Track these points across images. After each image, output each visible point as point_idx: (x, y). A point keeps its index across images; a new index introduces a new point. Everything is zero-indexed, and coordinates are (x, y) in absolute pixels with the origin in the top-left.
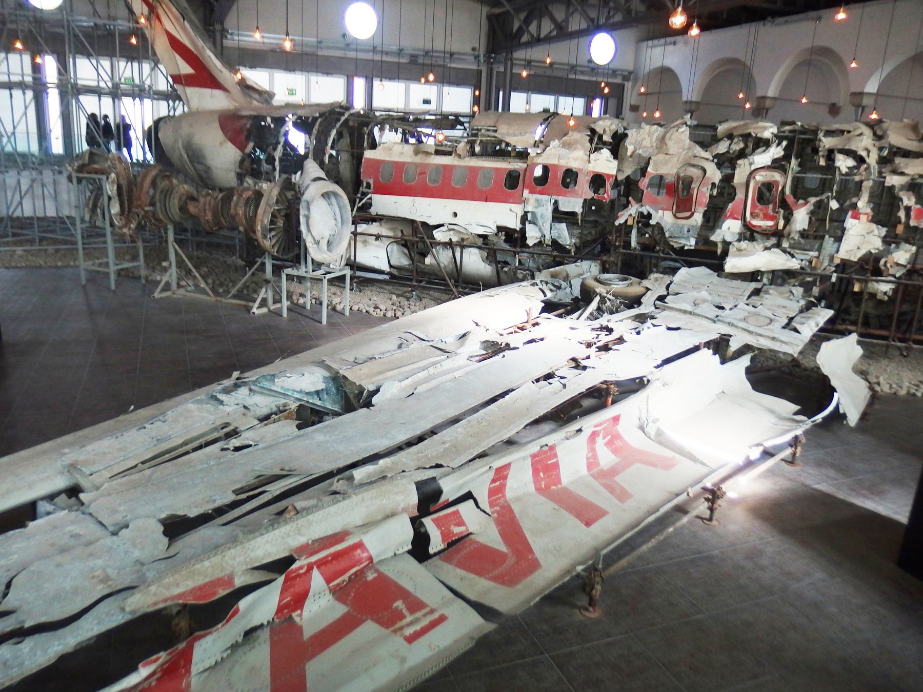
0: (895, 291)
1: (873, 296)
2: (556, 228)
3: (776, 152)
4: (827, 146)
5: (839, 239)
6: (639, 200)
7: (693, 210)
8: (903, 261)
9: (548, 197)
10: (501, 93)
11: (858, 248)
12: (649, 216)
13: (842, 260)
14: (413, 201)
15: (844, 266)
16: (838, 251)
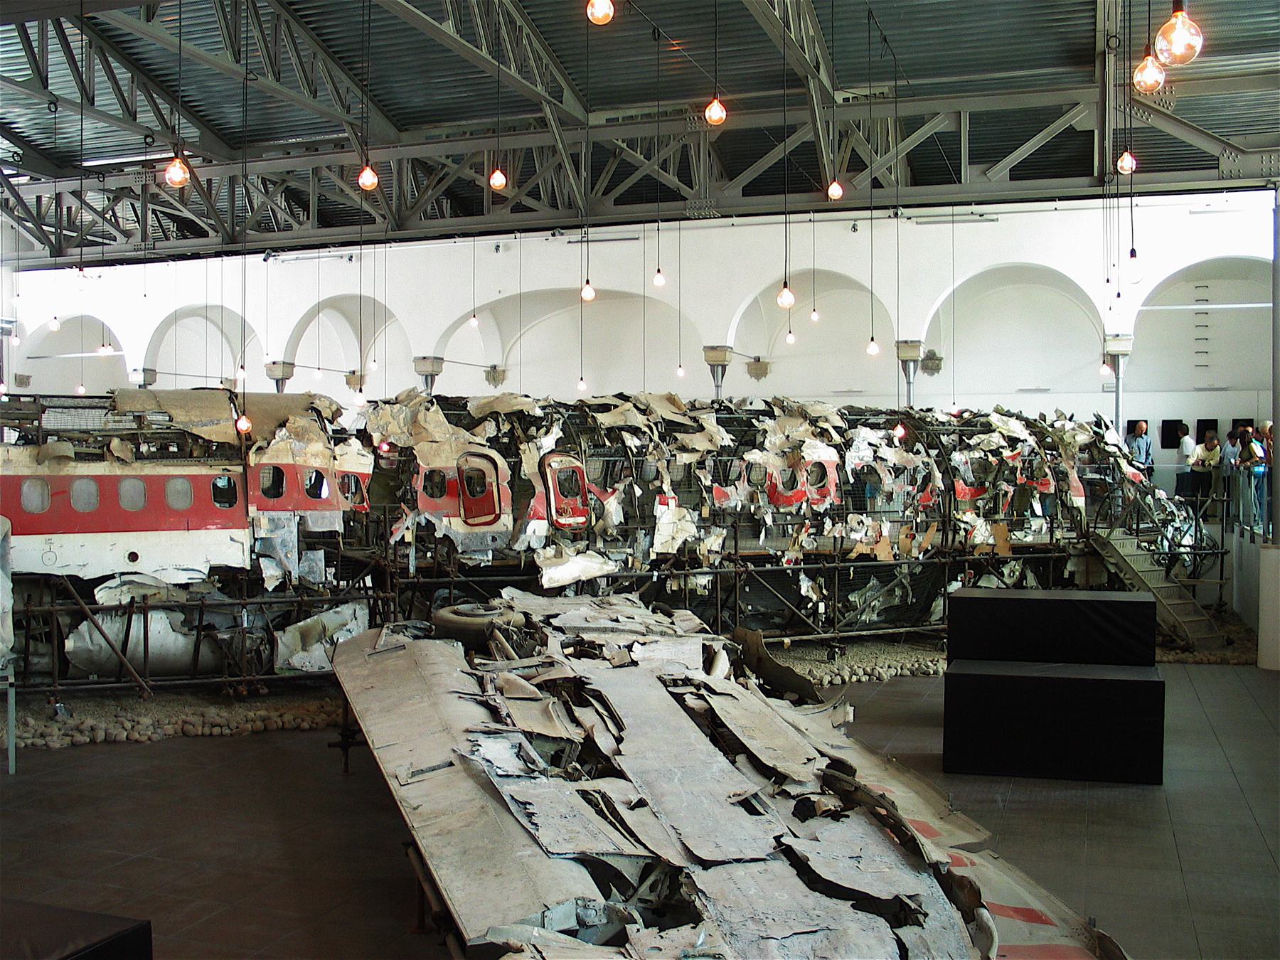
0: (714, 583)
1: (693, 591)
2: (308, 559)
3: (556, 432)
4: (607, 425)
5: (651, 532)
6: (414, 506)
7: (498, 512)
8: (716, 548)
9: (288, 514)
10: (1271, 526)
11: (673, 538)
12: (430, 526)
13: (657, 554)
14: (49, 542)
15: (663, 558)
16: (652, 545)
